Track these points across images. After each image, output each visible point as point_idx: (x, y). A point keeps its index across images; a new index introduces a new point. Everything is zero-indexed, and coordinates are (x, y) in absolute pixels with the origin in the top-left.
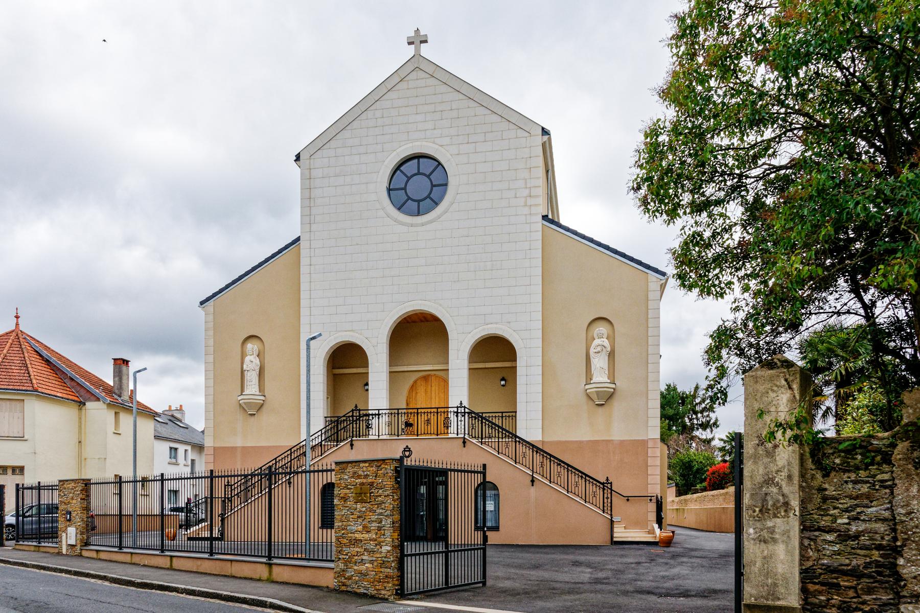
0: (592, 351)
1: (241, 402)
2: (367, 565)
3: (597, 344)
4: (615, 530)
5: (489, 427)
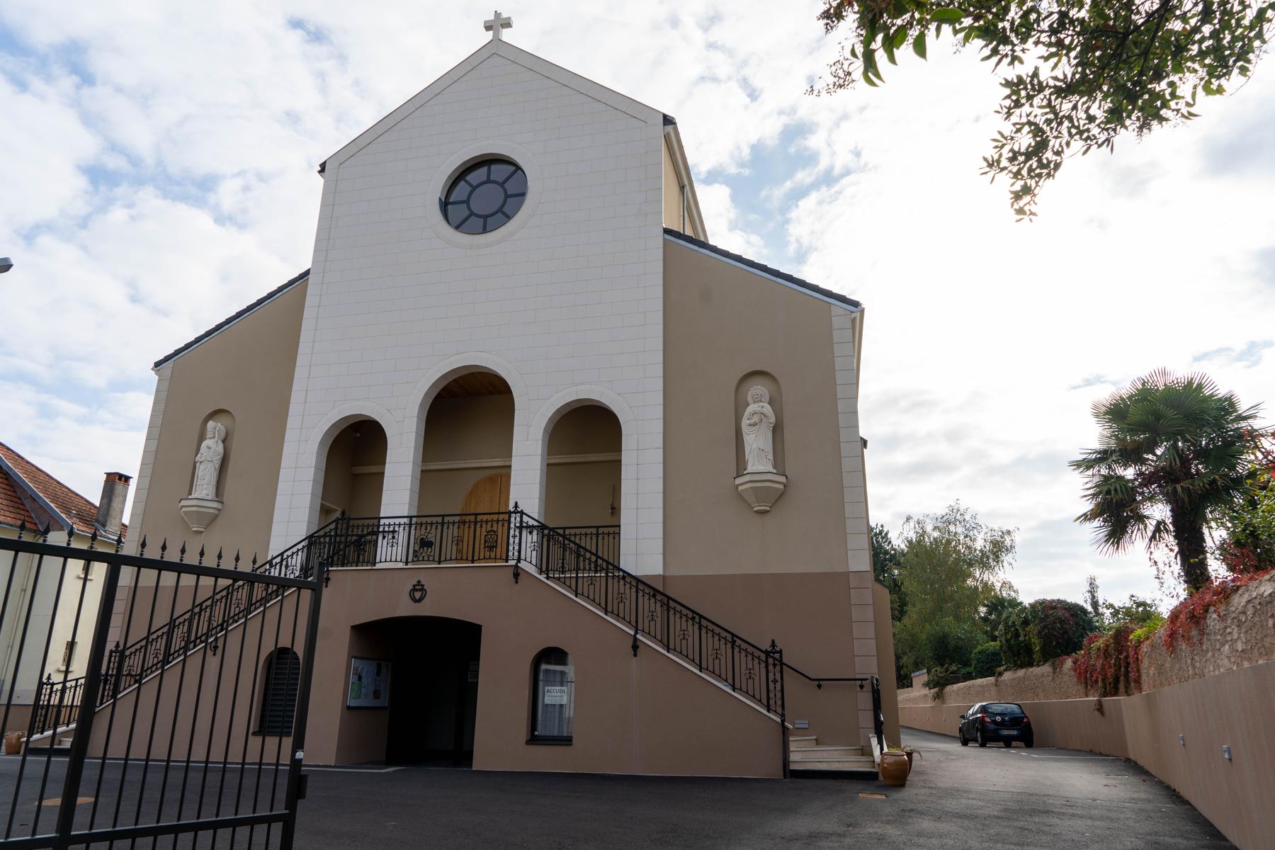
4: (792, 747)
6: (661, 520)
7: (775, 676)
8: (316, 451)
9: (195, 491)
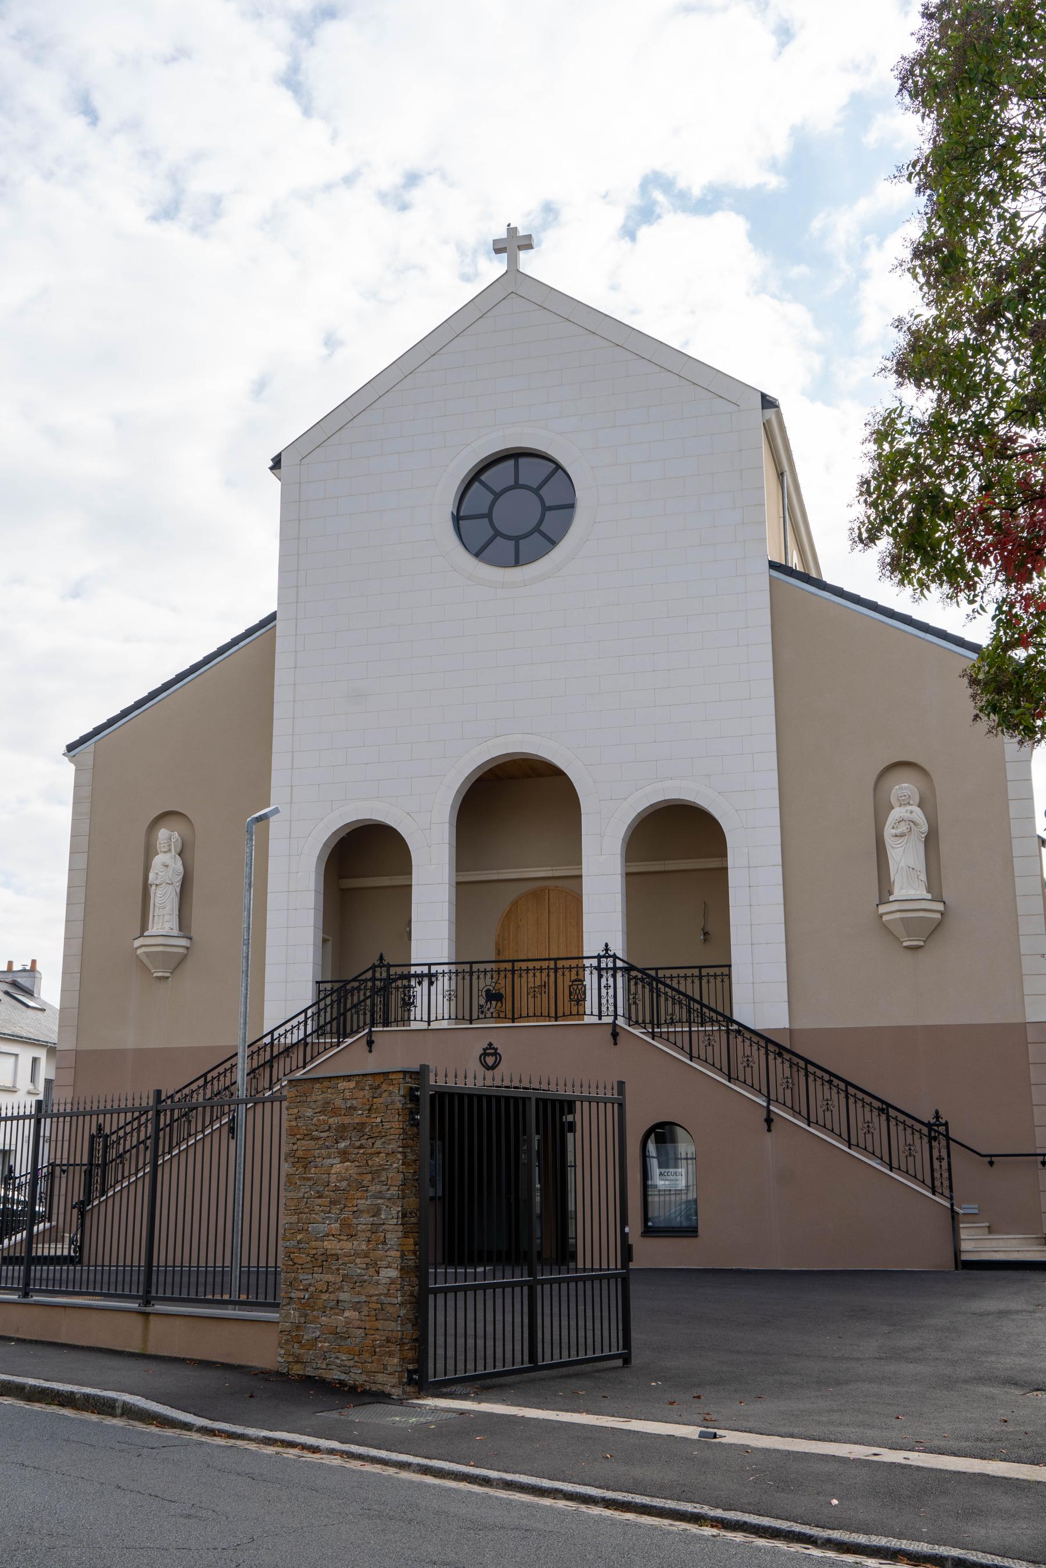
0: (888, 832)
1: (139, 952)
2: (347, 1314)
3: (897, 817)
4: (963, 1235)
5: (666, 1000)
6: (784, 959)
7: (940, 1152)
8: (314, 870)
9: (153, 924)
